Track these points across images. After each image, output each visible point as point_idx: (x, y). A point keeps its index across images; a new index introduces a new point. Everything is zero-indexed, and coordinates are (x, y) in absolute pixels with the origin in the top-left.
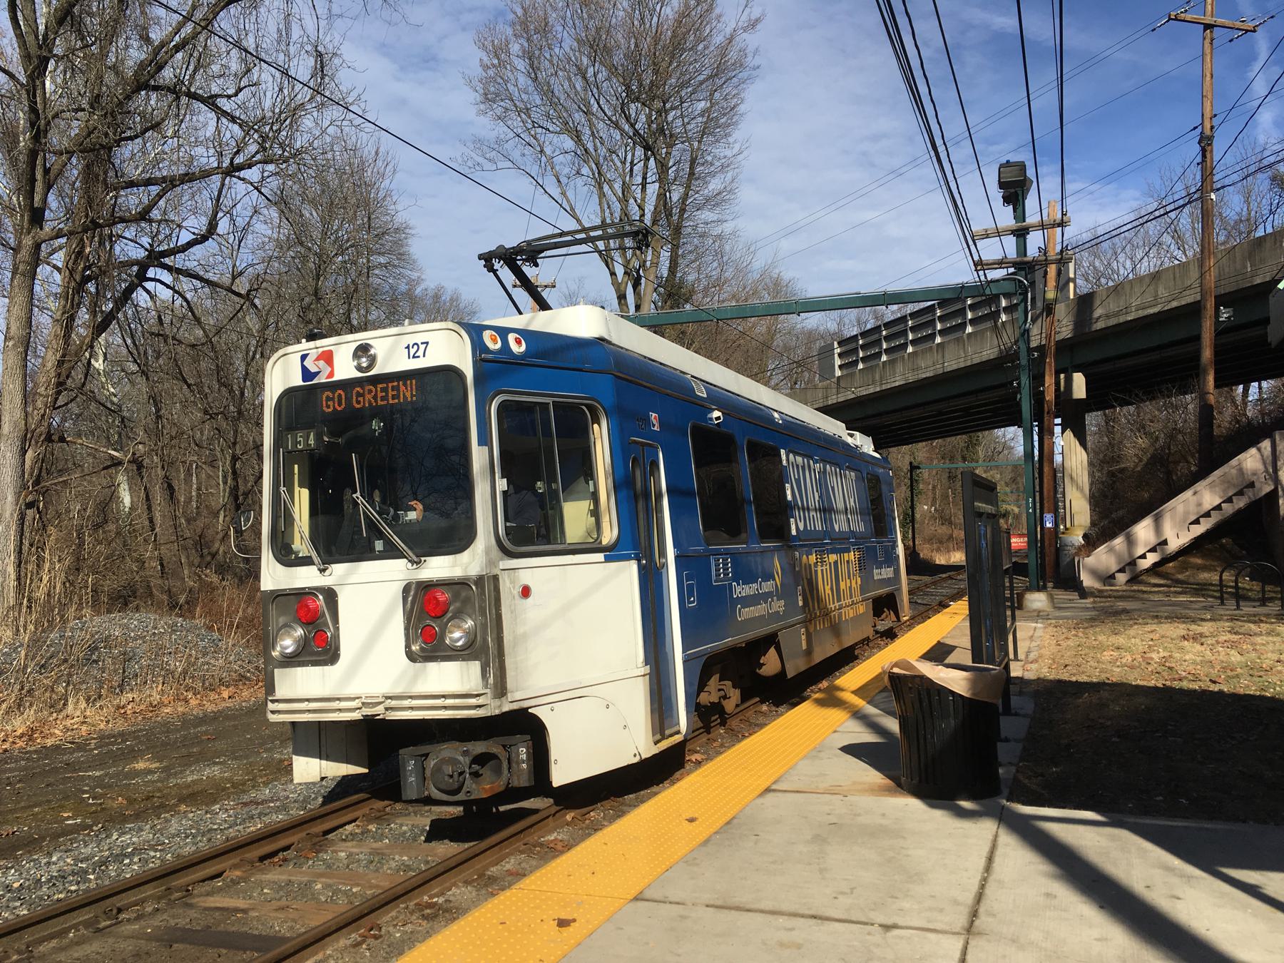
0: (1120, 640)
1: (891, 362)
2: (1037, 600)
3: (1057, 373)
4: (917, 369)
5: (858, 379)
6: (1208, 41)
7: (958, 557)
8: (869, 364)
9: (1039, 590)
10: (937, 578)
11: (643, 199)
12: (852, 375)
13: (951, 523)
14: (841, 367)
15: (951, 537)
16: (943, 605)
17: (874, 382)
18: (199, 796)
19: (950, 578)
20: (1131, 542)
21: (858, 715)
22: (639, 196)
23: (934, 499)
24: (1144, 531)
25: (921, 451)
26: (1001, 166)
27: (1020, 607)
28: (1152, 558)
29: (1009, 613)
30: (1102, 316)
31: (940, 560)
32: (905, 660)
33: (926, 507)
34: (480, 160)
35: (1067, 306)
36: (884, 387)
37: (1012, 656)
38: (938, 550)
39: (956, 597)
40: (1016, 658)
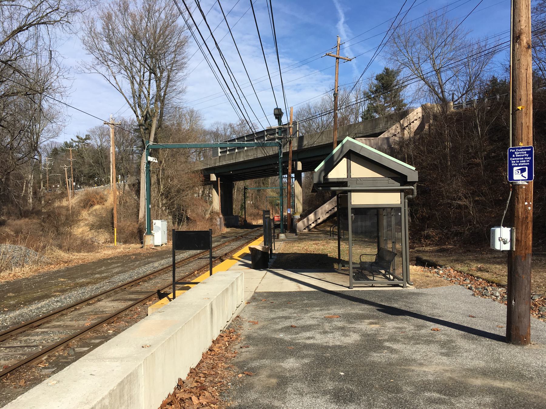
0: (300, 245)
1: (239, 152)
2: (282, 236)
3: (293, 161)
4: (248, 156)
5: (227, 158)
6: (337, 63)
7: (260, 222)
8: (231, 152)
9: (283, 233)
10: (254, 230)
11: (149, 88)
12: (225, 156)
13: (258, 208)
14: (220, 152)
15: (258, 214)
16: (256, 239)
17: (233, 159)
18: (82, 285)
19: (258, 230)
20: (308, 220)
21: (239, 261)
22: (147, 86)
23: (252, 199)
24: (312, 216)
25: (248, 182)
26: (275, 109)
27: (278, 238)
28: (313, 225)
29: (273, 240)
30: (306, 143)
31: (254, 223)
32: (244, 253)
33: (249, 202)
34: (85, 69)
35: (296, 139)
36: (236, 161)
37: (273, 248)
38: (254, 219)
39: (261, 236)
40: (275, 250)
